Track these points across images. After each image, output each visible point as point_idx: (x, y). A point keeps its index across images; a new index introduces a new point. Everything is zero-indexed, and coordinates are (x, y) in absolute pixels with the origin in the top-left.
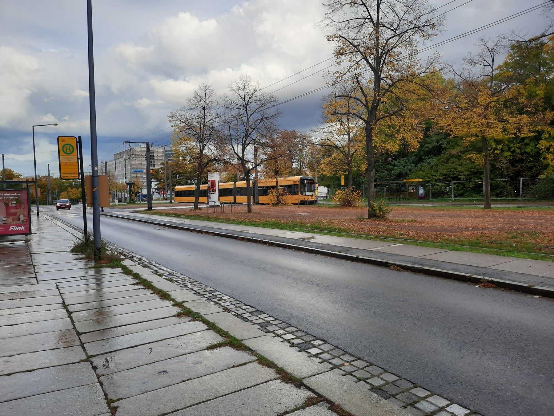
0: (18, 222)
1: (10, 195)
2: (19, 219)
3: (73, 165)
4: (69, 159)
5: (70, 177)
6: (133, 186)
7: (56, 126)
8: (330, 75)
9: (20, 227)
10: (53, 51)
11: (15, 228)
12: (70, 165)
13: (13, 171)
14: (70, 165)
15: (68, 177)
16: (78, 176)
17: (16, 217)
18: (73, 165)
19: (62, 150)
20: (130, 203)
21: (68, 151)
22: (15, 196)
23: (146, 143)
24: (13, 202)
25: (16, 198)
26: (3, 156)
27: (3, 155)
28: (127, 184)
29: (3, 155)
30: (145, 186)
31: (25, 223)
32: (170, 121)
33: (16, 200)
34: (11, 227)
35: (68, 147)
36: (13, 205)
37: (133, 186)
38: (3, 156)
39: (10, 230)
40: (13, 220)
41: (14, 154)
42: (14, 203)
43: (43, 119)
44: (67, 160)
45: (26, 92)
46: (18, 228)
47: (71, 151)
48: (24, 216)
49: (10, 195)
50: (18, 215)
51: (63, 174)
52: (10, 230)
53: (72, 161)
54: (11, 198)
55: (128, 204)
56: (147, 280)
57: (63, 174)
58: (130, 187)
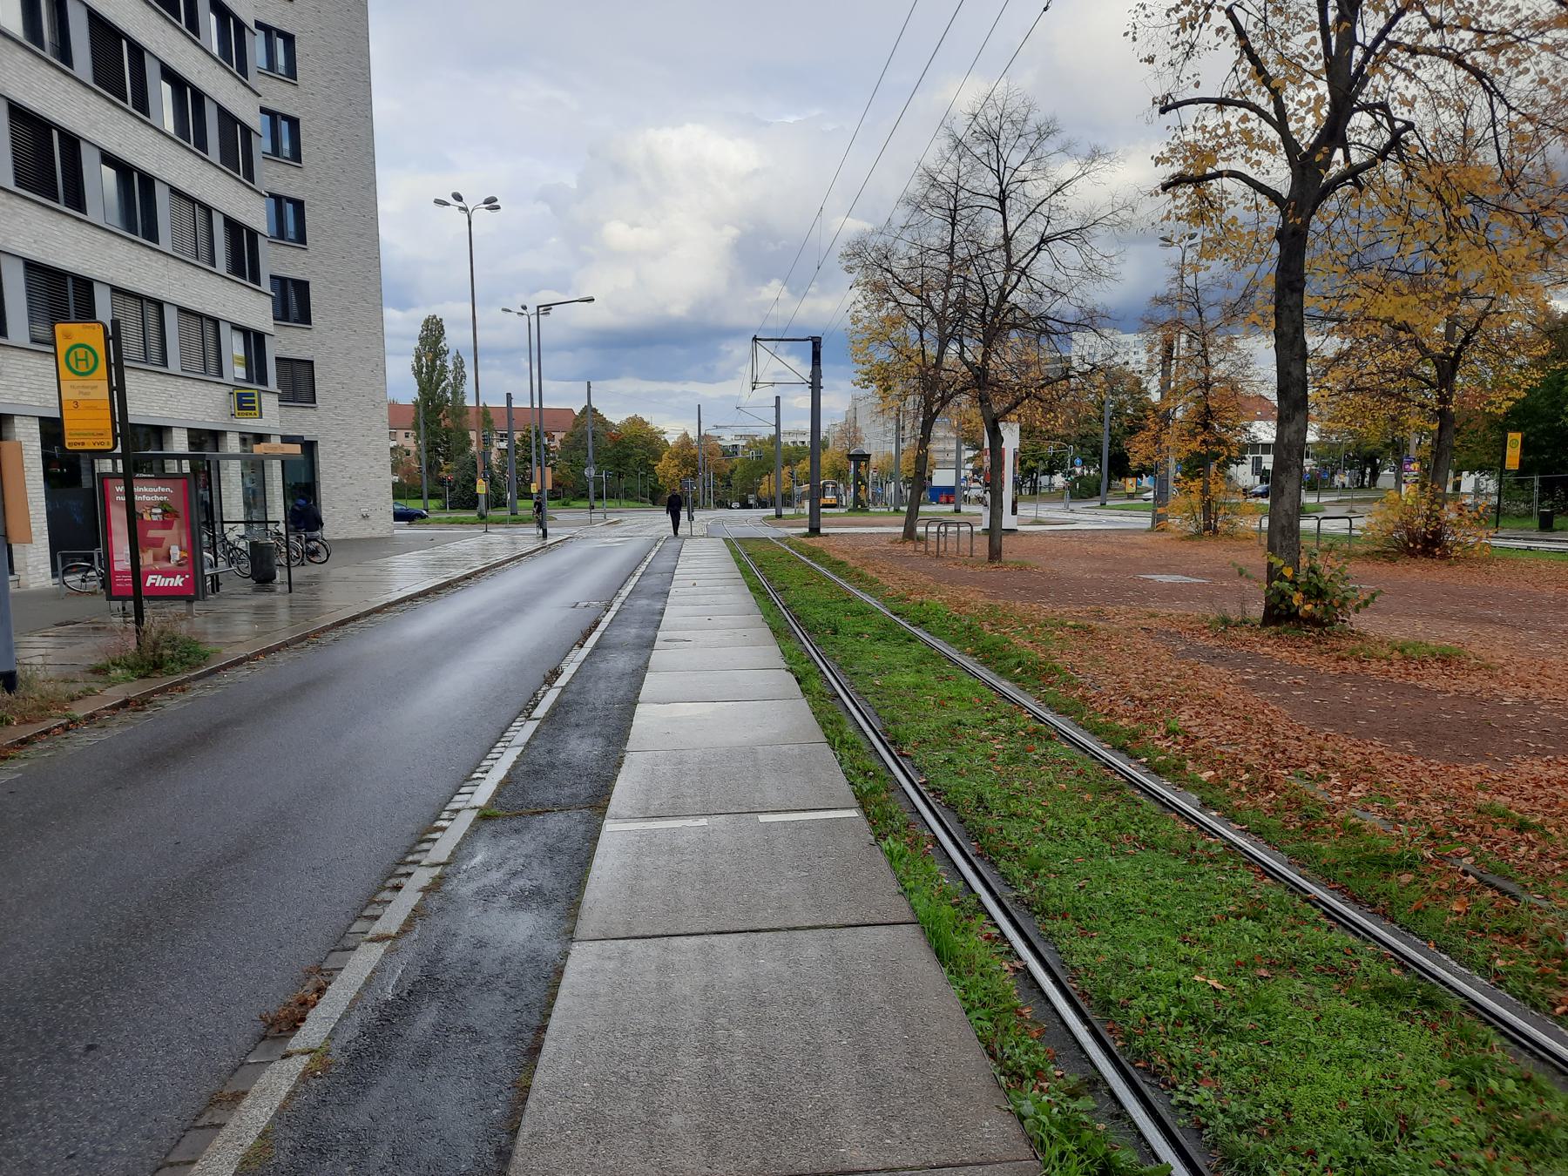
0: (167, 565)
1: (146, 490)
2: (168, 559)
3: (95, 408)
4: (86, 390)
5: (89, 444)
6: (863, 464)
7: (591, 304)
8: (1153, 21)
9: (172, 579)
10: (791, 119)
11: (161, 582)
12: (88, 408)
13: (647, 424)
14: (88, 408)
15: (83, 444)
16: (111, 441)
17: (161, 551)
18: (95, 408)
19: (64, 363)
20: (854, 510)
21: (82, 368)
22: (159, 494)
23: (813, 339)
24: (154, 511)
25: (161, 498)
26: (589, 387)
27: (589, 383)
28: (850, 457)
29: (589, 383)
30: (950, 462)
31: (186, 568)
32: (849, 270)
33: (162, 504)
34: (150, 577)
35: (81, 352)
36: (155, 518)
37: (863, 464)
38: (589, 387)
39: (148, 584)
40: (155, 559)
41: (696, 381)
42: (155, 514)
43: (760, 293)
44: (80, 393)
45: (731, 232)
46: (168, 580)
47: (91, 366)
48: (181, 550)
49: (146, 490)
50: (165, 544)
51: (70, 434)
52: (148, 584)
53: (95, 395)
54: (148, 498)
55: (851, 513)
56: (515, 762)
57: (70, 434)
58: (857, 467)
